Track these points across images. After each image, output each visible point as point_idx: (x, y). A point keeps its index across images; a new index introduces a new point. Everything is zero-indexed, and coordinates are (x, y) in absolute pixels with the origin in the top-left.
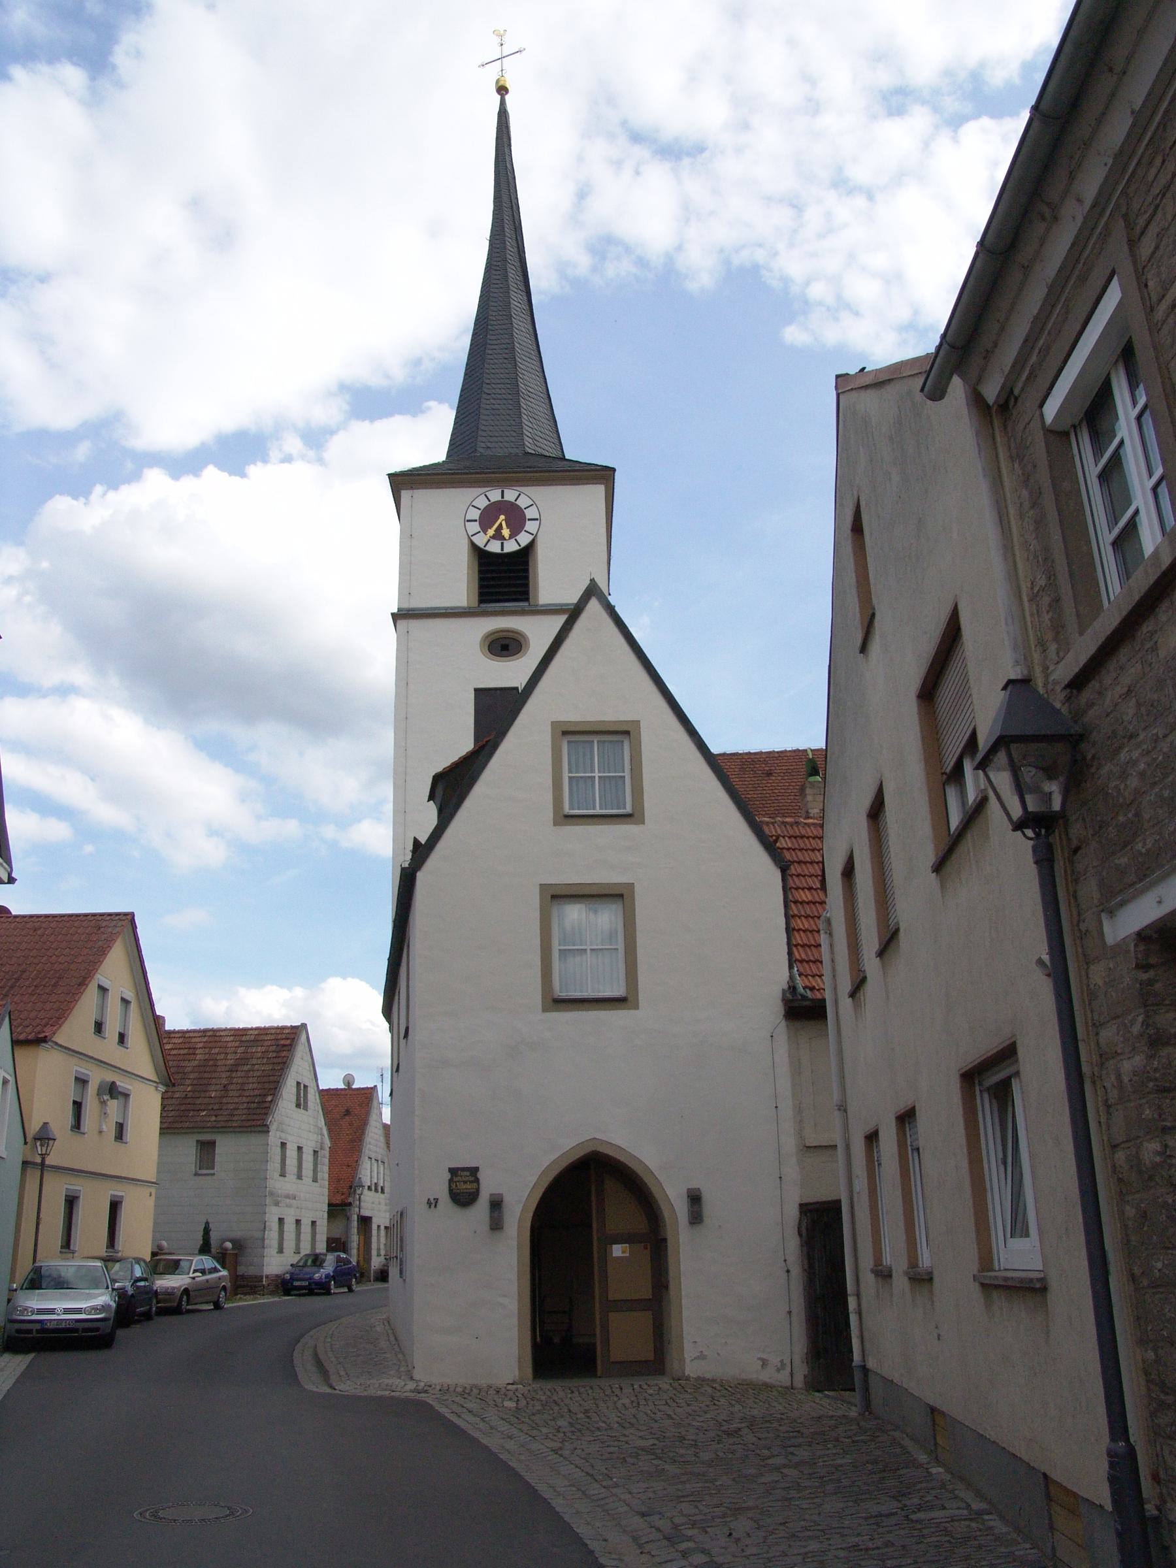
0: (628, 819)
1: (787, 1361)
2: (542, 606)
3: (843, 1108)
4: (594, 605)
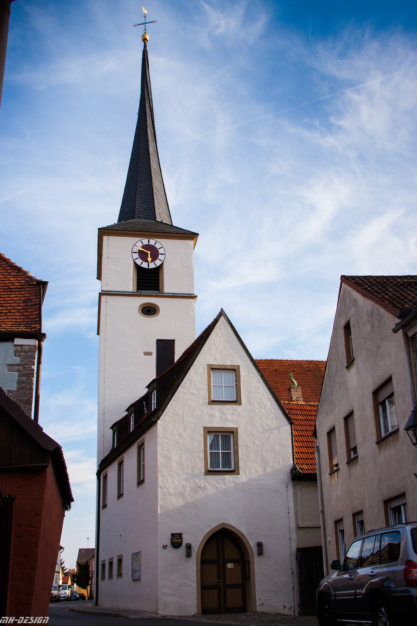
0: (235, 403)
1: (292, 606)
2: (165, 294)
3: (323, 512)
4: (222, 318)
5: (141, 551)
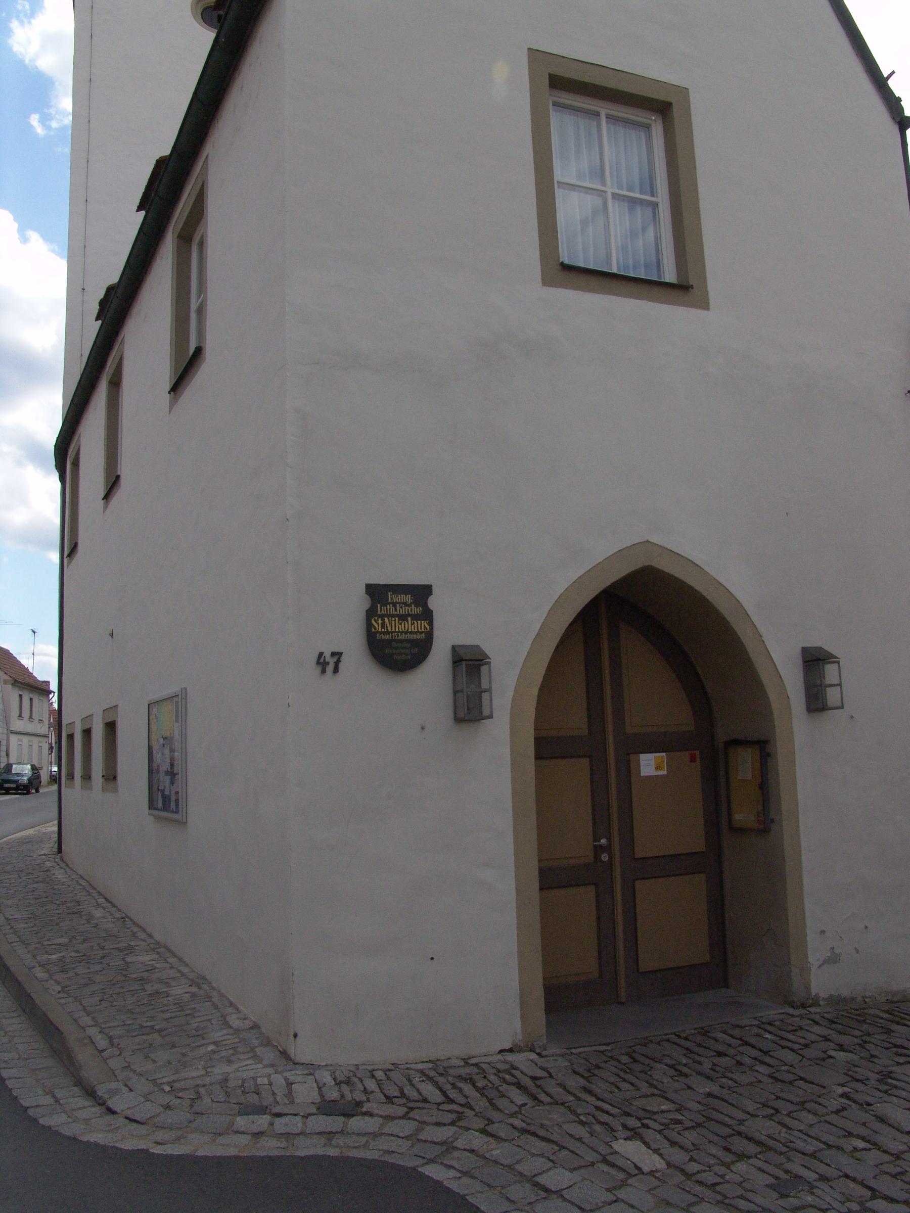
5: (184, 691)
